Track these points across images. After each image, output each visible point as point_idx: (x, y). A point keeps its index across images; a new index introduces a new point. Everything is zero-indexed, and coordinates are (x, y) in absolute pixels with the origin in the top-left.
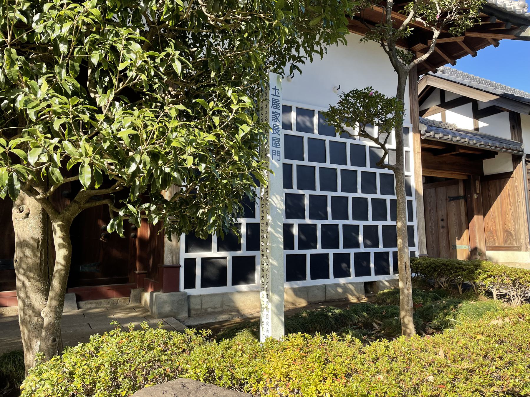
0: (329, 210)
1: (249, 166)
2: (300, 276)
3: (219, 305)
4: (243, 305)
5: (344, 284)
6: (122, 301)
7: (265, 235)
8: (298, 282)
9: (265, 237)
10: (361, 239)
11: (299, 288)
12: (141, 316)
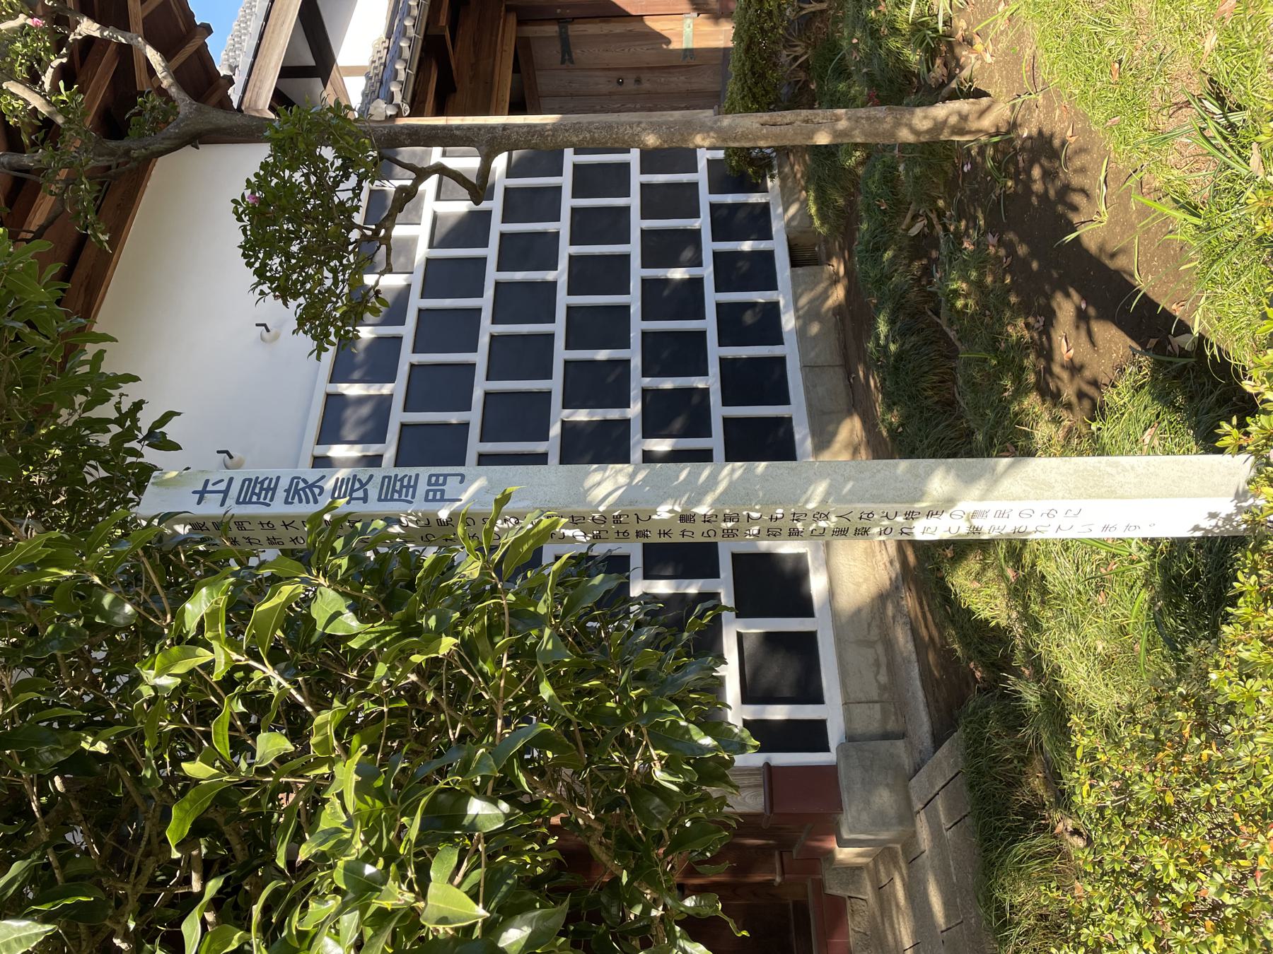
0: (602, 355)
1: (478, 591)
2: (781, 431)
4: (864, 586)
5: (797, 318)
6: (858, 918)
7: (724, 525)
8: (797, 437)
9: (730, 525)
10: (678, 274)
11: (813, 436)
12: (904, 871)
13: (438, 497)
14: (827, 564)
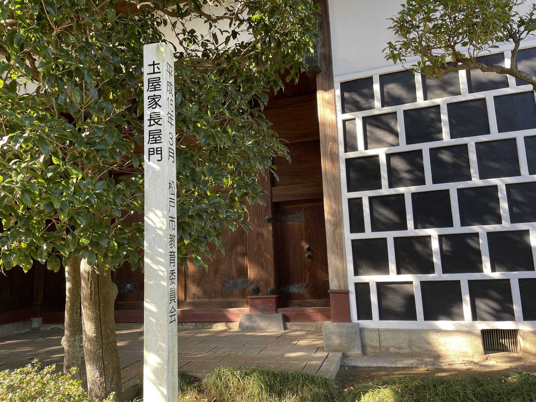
3: (405, 345)
13: (151, 153)
14: (458, 331)
